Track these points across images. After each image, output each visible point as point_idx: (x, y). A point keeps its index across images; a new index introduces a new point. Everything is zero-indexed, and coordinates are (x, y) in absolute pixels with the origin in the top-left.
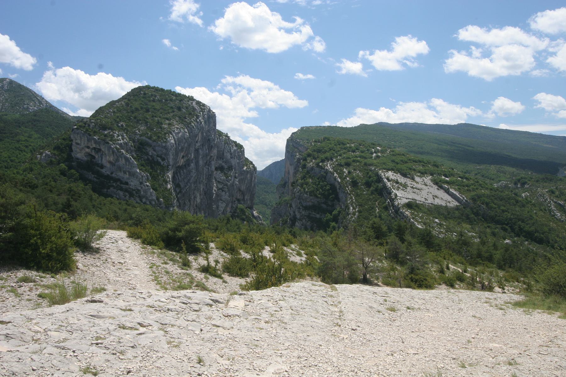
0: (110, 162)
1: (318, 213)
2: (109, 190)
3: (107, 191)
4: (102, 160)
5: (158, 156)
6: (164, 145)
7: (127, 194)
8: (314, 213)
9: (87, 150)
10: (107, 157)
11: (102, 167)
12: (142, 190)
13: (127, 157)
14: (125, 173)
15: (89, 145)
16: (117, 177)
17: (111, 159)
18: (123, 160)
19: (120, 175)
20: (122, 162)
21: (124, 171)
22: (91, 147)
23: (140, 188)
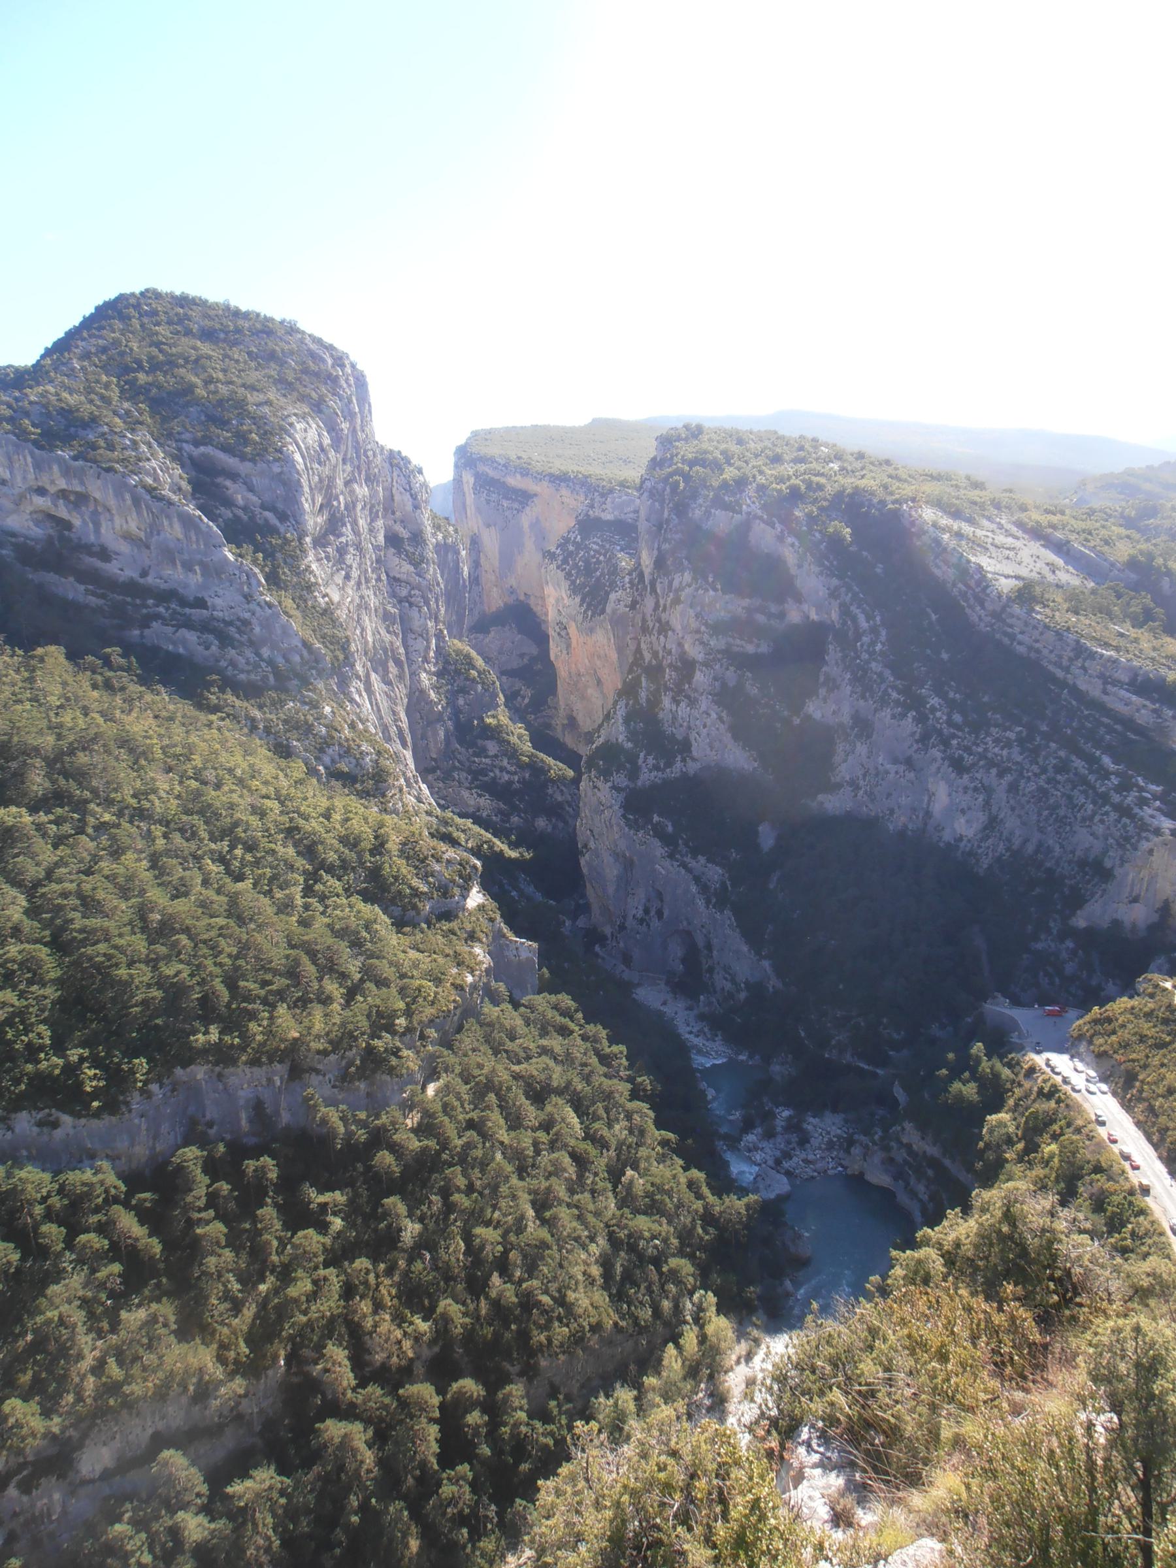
0: (127, 537)
1: (751, 642)
2: (147, 632)
3: (142, 636)
4: (97, 525)
5: (264, 507)
6: (276, 469)
7: (211, 637)
8: (738, 642)
9: (40, 502)
10: (118, 521)
11: (104, 554)
12: (254, 621)
13: (188, 514)
14: (188, 567)
15: (44, 481)
16: (163, 586)
17: (133, 526)
18: (177, 526)
19: (175, 576)
20: (174, 531)
21: (184, 565)
22: (52, 489)
23: (247, 615)
